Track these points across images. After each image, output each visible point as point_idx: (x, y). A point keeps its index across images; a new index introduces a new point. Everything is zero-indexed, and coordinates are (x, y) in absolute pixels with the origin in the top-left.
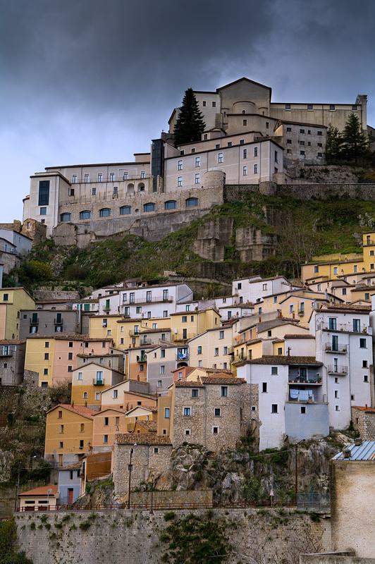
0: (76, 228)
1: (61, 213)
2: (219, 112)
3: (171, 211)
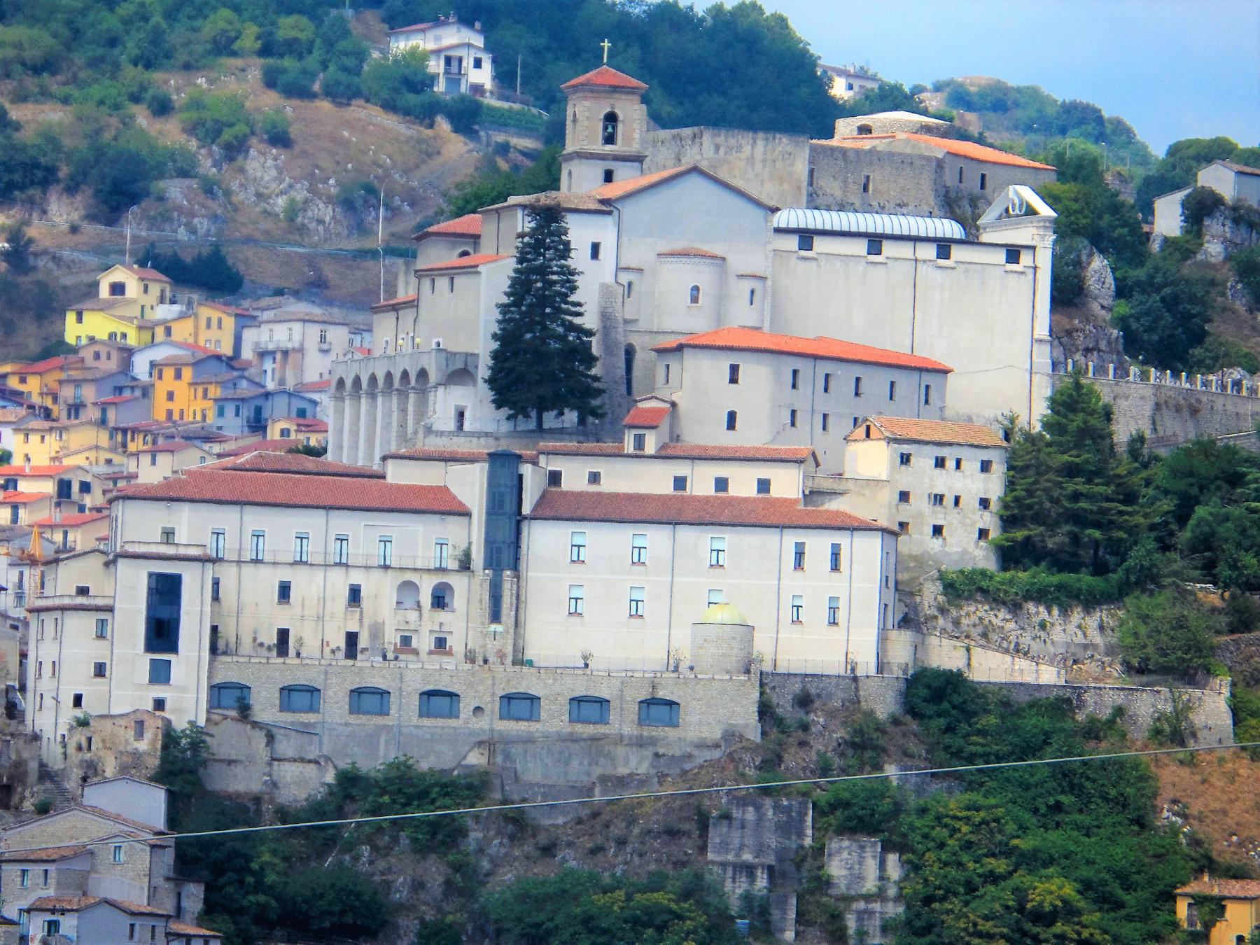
0: (271, 738)
1: (217, 681)
2: (609, 279)
3: (589, 730)
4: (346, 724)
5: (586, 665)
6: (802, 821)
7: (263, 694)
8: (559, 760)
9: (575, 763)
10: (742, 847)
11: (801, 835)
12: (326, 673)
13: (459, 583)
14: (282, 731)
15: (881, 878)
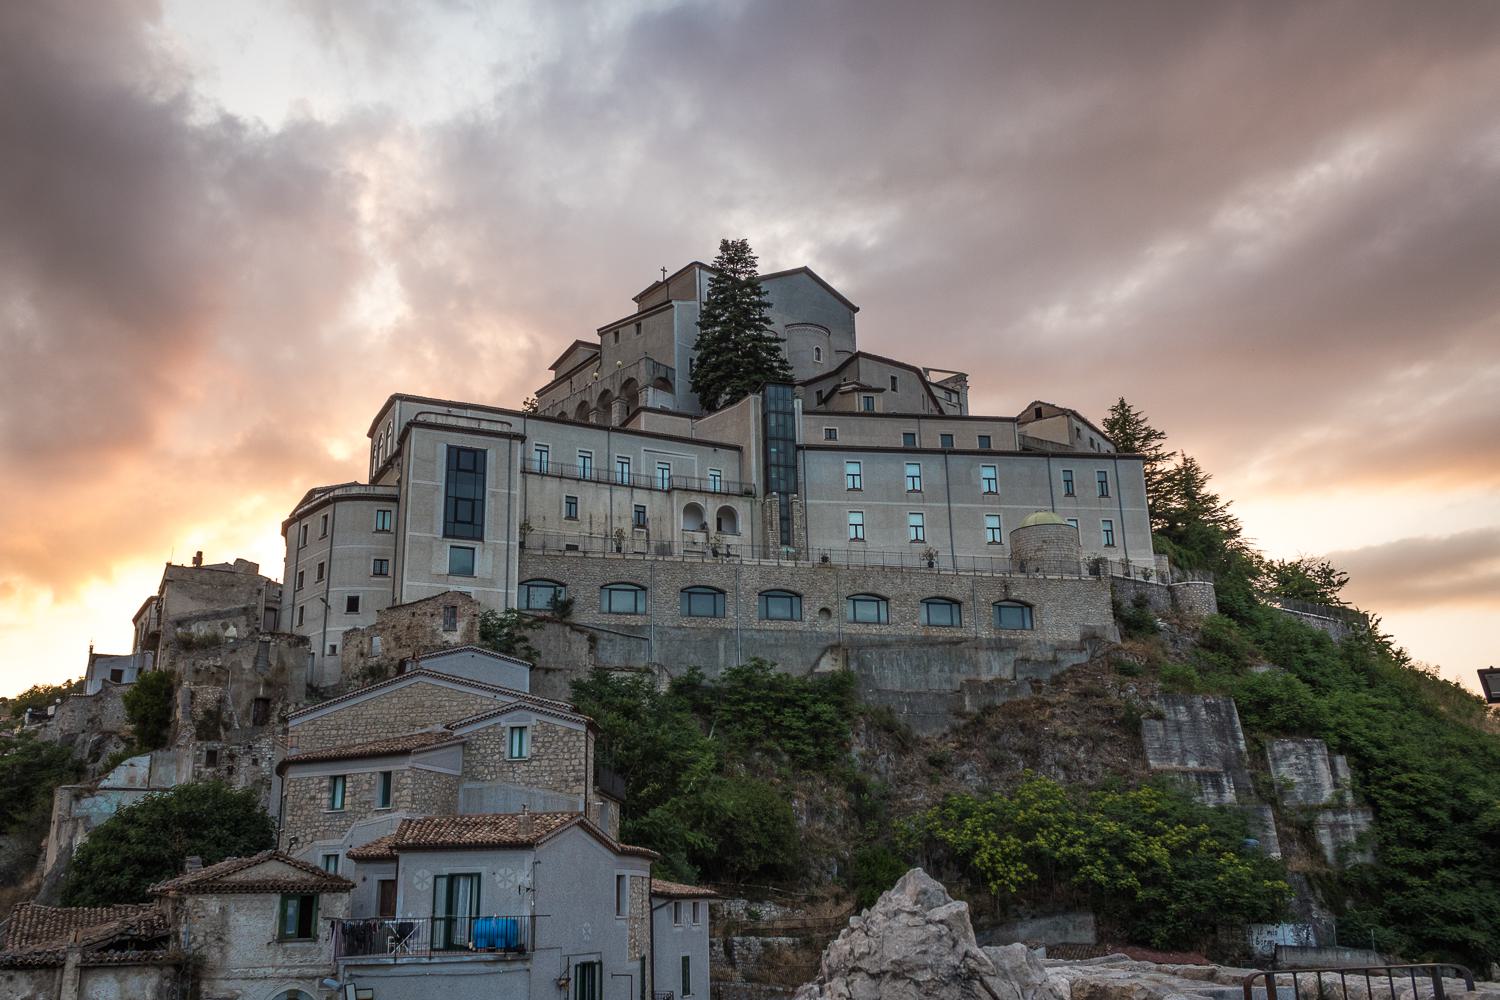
4: (679, 628)
5: (931, 565)
6: (1232, 722)
7: (582, 592)
8: (918, 666)
9: (935, 670)
10: (1185, 752)
11: (1236, 739)
12: (652, 568)
13: (742, 508)
14: (606, 635)
15: (1336, 785)
